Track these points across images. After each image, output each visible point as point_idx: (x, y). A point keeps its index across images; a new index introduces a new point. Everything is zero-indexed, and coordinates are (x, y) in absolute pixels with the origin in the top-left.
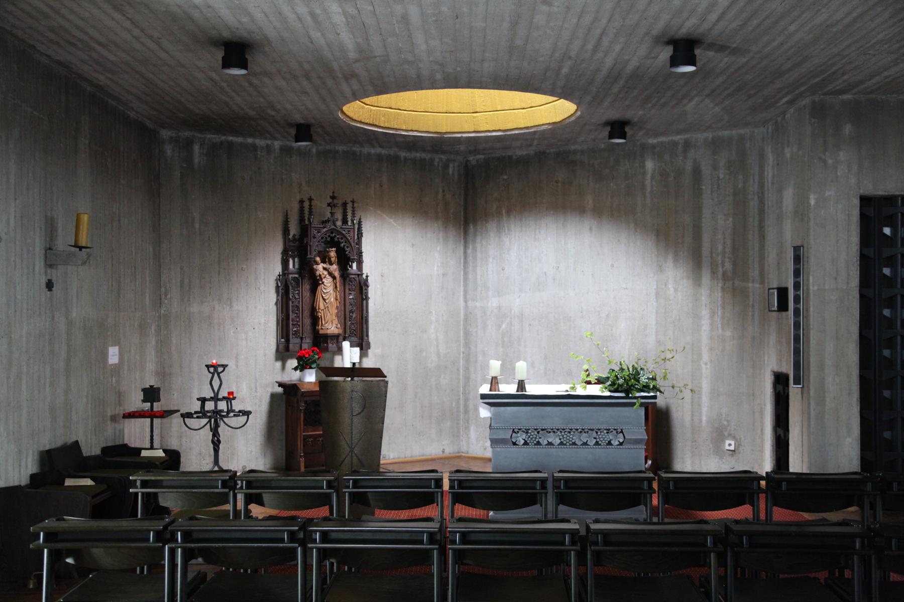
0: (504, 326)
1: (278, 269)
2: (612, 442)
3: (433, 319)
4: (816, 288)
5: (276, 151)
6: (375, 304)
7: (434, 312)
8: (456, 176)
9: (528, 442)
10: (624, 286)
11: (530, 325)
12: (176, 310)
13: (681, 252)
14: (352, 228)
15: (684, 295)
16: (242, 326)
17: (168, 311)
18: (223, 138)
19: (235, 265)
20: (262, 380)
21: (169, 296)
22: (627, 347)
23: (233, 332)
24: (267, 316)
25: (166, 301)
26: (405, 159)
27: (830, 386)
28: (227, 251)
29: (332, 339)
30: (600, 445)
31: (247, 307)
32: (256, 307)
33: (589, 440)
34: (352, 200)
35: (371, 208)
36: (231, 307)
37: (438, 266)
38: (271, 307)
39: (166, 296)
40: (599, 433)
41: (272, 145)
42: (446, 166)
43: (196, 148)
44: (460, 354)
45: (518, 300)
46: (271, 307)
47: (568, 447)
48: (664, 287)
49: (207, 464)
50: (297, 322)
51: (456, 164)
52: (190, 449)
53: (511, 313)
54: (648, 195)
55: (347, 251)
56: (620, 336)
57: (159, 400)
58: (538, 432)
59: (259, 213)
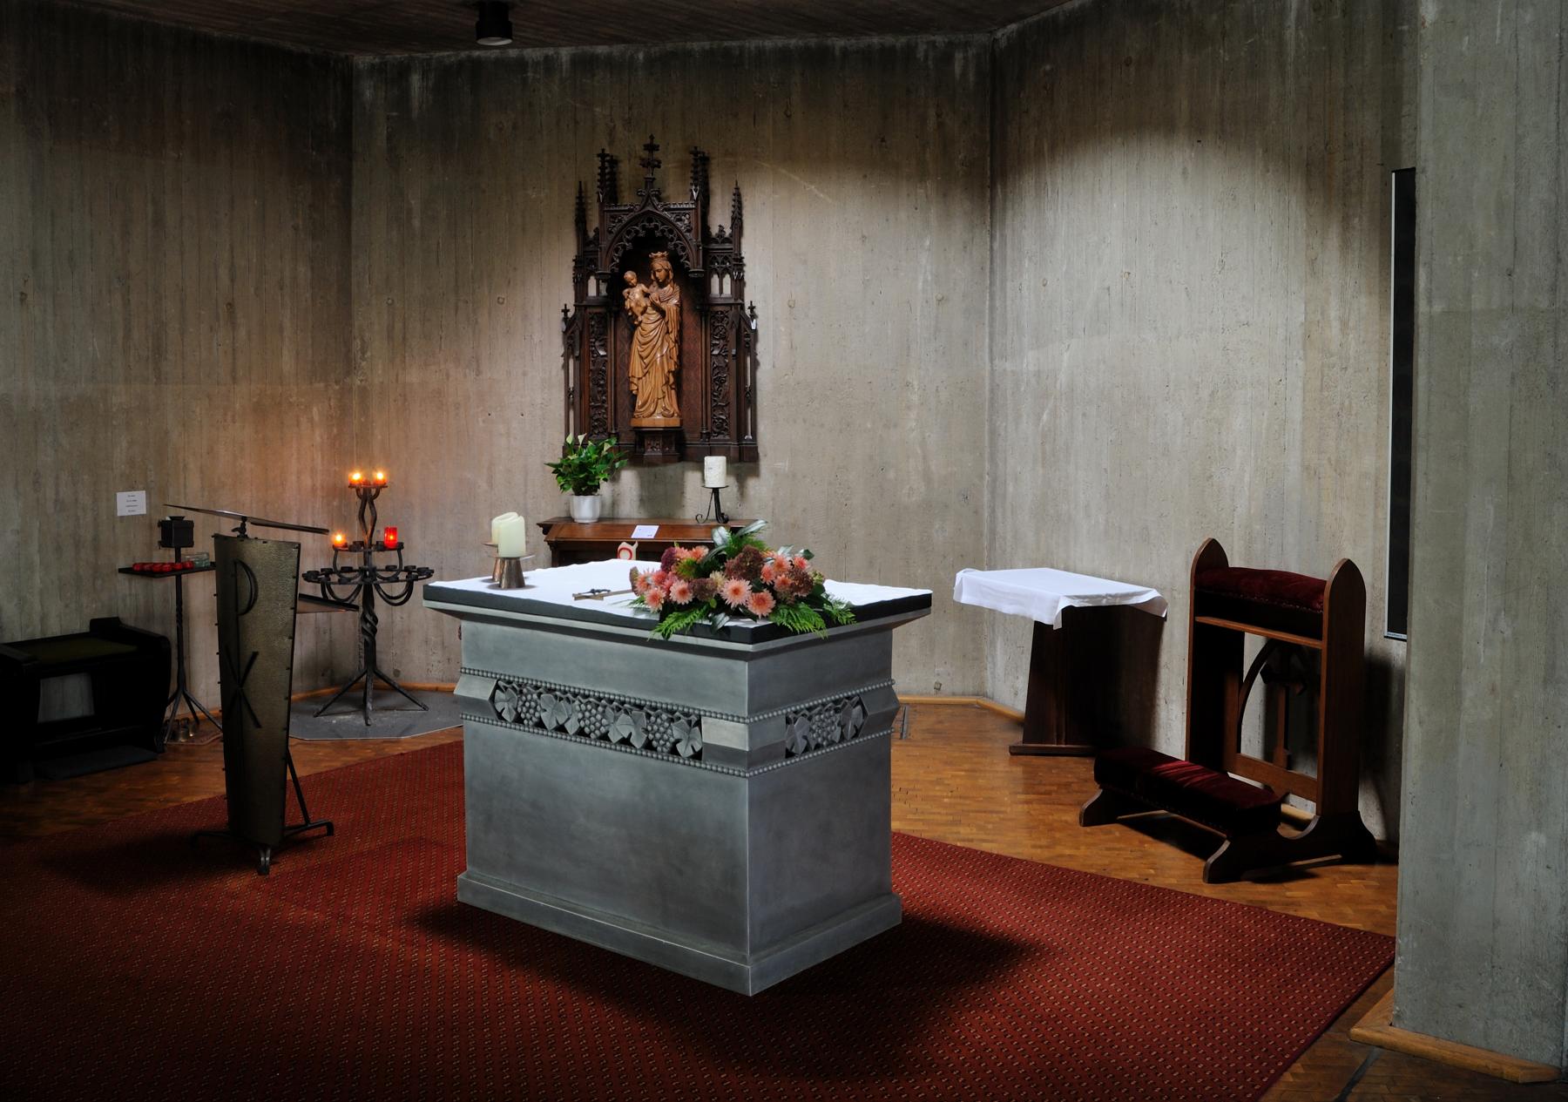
0: (1045, 417)
1: (568, 298)
2: (679, 747)
3: (915, 398)
4: (1438, 308)
5: (564, 67)
6: (774, 367)
7: (915, 383)
8: (971, 77)
9: (523, 716)
10: (1243, 318)
11: (1084, 415)
12: (381, 380)
13: (1356, 220)
14: (692, 209)
15: (1361, 339)
16: (499, 409)
17: (366, 380)
18: (463, 54)
19: (486, 293)
20: (539, 513)
21: (369, 354)
22: (1247, 479)
23: (484, 421)
24: (546, 391)
25: (364, 363)
26: (845, 52)
27: (1481, 646)
28: (471, 267)
29: (654, 439)
30: (655, 749)
31: (509, 373)
32: (525, 374)
33: (634, 734)
34: (600, 152)
35: (766, 165)
36: (479, 373)
37: (925, 281)
38: (554, 373)
39: (363, 353)
40: (653, 719)
41: (555, 56)
42: (946, 58)
43: (416, 80)
44: (981, 477)
45: (1066, 356)
46: (554, 373)
47: (613, 747)
48: (1319, 317)
49: (439, 662)
50: (604, 402)
51: (971, 52)
52: (409, 632)
53: (1055, 387)
54: (1290, 69)
55: (682, 256)
56: (1234, 450)
57: (190, 544)
58: (539, 695)
59: (530, 192)
